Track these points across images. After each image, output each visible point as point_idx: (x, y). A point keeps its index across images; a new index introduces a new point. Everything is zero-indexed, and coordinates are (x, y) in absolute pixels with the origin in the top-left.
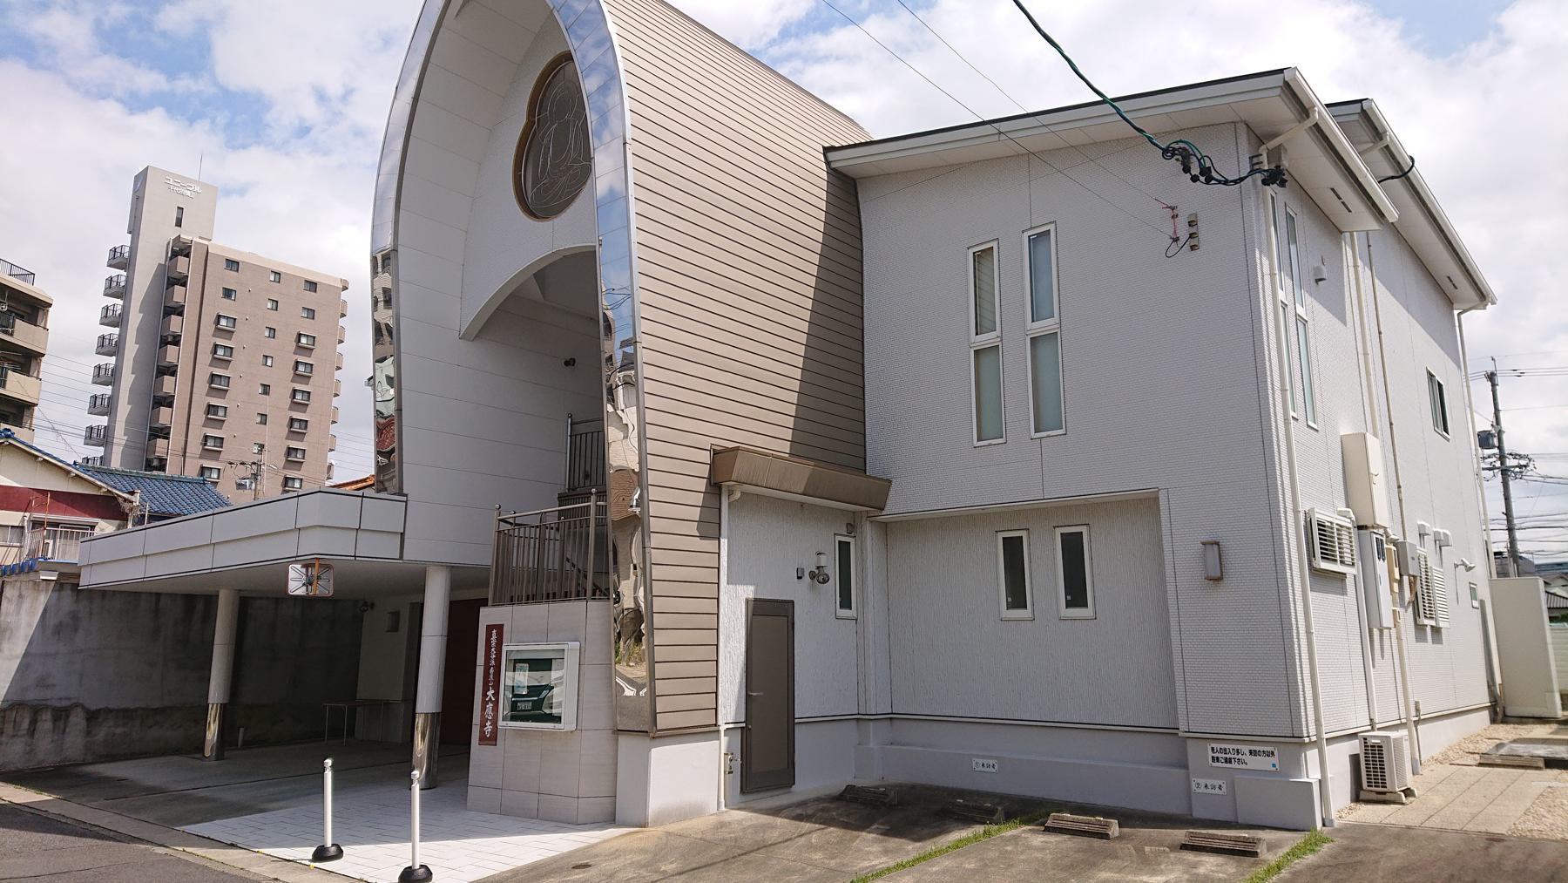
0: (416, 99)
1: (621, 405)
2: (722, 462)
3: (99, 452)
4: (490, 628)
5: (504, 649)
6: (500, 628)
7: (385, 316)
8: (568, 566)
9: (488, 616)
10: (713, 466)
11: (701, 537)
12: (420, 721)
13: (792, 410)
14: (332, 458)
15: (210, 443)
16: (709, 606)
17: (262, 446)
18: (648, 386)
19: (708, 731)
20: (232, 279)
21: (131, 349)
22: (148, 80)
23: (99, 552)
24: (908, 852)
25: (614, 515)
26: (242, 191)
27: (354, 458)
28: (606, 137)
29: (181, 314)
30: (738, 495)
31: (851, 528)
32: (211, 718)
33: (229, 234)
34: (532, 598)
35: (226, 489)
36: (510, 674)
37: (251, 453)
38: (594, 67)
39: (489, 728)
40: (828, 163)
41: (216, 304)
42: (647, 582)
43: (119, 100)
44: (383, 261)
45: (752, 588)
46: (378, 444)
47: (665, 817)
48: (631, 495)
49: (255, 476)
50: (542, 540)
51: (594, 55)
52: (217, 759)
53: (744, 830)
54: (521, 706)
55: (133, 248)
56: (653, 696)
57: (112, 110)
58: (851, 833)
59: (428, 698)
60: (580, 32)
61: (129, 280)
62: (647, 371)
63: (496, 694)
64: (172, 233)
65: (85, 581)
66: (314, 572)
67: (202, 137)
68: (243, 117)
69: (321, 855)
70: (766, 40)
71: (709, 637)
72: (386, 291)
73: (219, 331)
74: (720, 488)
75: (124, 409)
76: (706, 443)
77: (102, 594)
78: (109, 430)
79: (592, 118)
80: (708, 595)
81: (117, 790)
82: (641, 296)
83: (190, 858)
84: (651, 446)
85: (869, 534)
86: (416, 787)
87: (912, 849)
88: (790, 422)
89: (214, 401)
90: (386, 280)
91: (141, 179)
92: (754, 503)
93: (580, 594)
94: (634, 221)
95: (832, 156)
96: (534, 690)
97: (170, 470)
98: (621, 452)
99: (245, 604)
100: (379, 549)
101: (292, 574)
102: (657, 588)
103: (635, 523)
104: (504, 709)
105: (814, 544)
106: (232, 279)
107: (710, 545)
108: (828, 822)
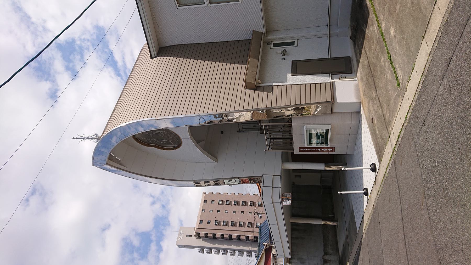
0: (151, 177)
1: (233, 117)
2: (250, 86)
3: (253, 254)
4: (300, 151)
5: (306, 146)
6: (300, 148)
7: (212, 183)
8: (281, 130)
9: (296, 151)
10: (251, 89)
11: (273, 91)
12: (327, 169)
13: (232, 65)
14: (252, 194)
15: (249, 225)
16: (294, 87)
17: (250, 212)
18: (228, 110)
19: (332, 85)
20: (205, 222)
21: (225, 246)
22: (153, 247)
23: (281, 253)
24: (373, 17)
25: (266, 118)
26: (181, 221)
27: (253, 189)
28: (156, 125)
29: (215, 234)
30: (259, 81)
31: (269, 43)
32: (326, 224)
33: (193, 223)
34: (291, 140)
35: (262, 221)
36: (313, 145)
37: (252, 215)
38: (136, 129)
39: (330, 150)
40: (155, 57)
41: (212, 225)
42: (286, 107)
43: (159, 253)
44: (197, 184)
45: (288, 74)
46: (248, 183)
47: (358, 97)
48: (260, 113)
49: (258, 214)
50: (274, 138)
51: (133, 129)
52: (337, 221)
53: (363, 72)
54: (323, 141)
55: (198, 247)
56: (321, 103)
57: (162, 256)
58: (366, 37)
59: (321, 167)
60: (127, 133)
61: (207, 248)
62: (223, 110)
63: (319, 148)
64: (193, 238)
65: (288, 256)
66: (285, 198)
67: (167, 232)
68: (161, 223)
69: (366, 194)
70: (122, 81)
71: (303, 87)
72: (205, 183)
73: (219, 224)
74: (257, 86)
75: (242, 248)
76: (244, 91)
77: (292, 252)
78: (247, 251)
79: (151, 129)
80: (291, 87)
81: (347, 247)
82: (201, 113)
83: (367, 228)
84: (246, 108)
85: (270, 37)
86: (347, 169)
87: (372, 16)
88: (236, 65)
89: (238, 225)
90: (202, 183)
91: (180, 246)
92: (262, 76)
93: (290, 126)
94: (179, 116)
95: (153, 56)
96: (318, 137)
97: (257, 235)
98: (247, 117)
99: (293, 215)
100: (278, 182)
101: (285, 204)
102: (288, 104)
103: (268, 111)
104: (324, 146)
105: (274, 54)
106: (205, 222)
107: (275, 89)
108: (362, 44)
